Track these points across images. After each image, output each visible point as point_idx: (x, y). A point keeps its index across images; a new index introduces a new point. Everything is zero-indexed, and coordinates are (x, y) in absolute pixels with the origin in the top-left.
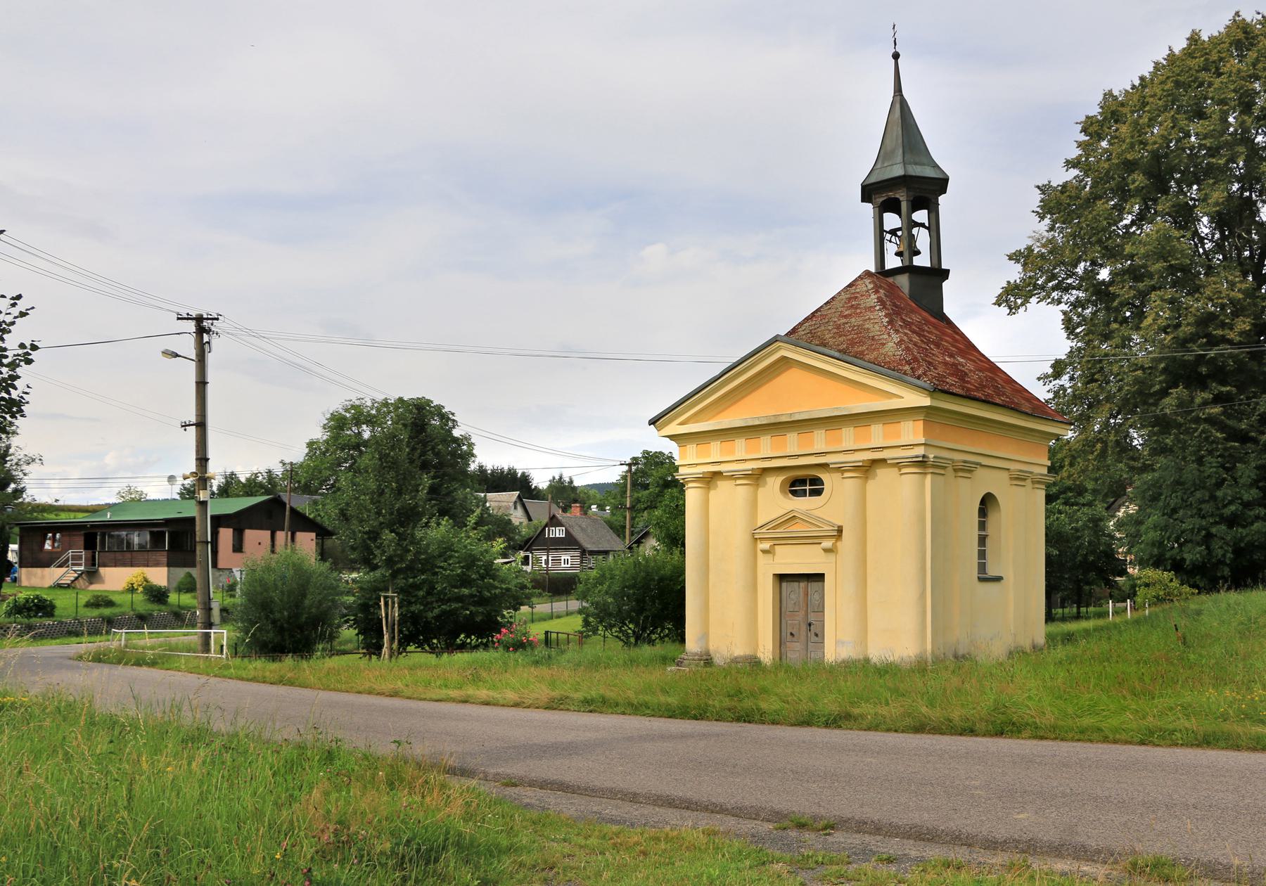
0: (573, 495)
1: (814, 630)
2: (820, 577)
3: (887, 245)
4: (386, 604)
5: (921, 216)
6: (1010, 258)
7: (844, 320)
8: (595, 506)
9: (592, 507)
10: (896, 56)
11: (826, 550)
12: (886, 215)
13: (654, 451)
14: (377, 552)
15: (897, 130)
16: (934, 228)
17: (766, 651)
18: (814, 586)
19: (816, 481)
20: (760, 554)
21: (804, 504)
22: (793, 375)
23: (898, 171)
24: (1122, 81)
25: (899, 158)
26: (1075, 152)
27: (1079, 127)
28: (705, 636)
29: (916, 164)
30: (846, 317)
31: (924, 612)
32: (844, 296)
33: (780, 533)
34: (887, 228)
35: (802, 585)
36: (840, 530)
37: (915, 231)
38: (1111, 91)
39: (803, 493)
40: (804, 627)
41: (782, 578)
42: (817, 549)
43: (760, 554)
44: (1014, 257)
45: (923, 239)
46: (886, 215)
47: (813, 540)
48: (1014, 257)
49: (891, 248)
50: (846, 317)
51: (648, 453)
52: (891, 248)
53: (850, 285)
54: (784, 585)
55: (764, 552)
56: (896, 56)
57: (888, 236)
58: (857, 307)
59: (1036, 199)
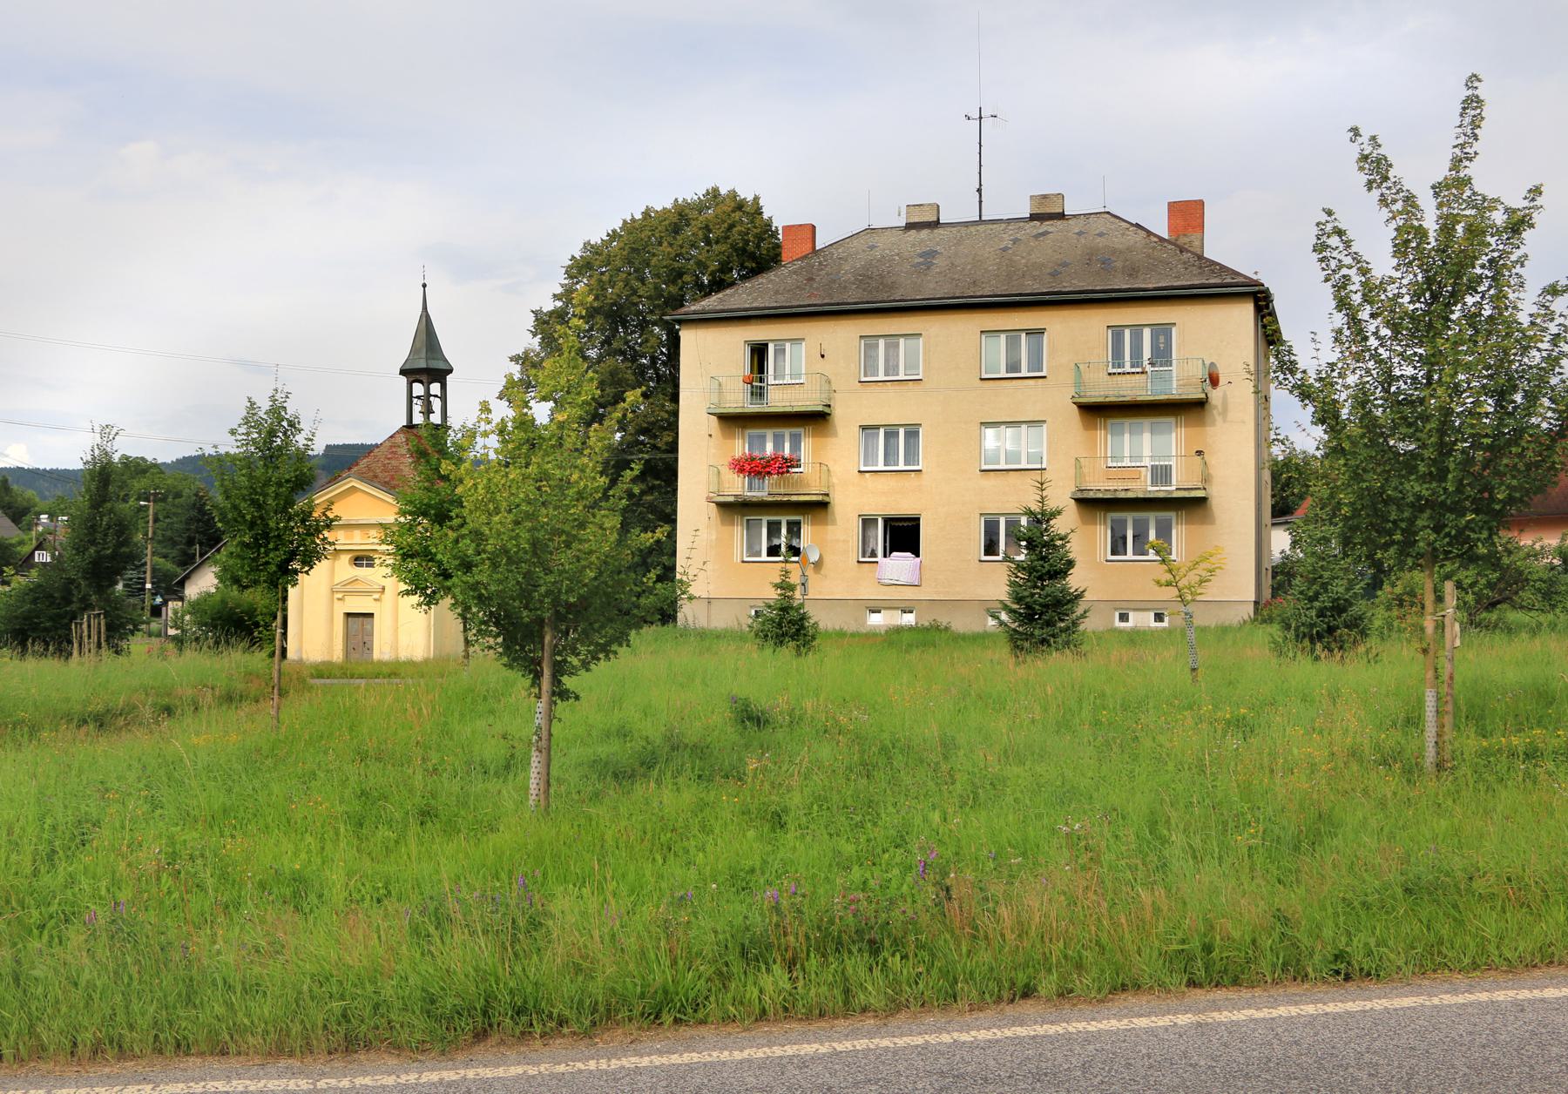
0: (7, 498)
1: (367, 645)
2: (371, 615)
3: (415, 407)
4: (76, 627)
5: (435, 388)
6: (511, 359)
7: (388, 461)
8: (46, 516)
9: (42, 516)
10: (424, 286)
11: (375, 600)
12: (415, 385)
13: (134, 456)
14: (75, 592)
15: (424, 336)
16: (443, 398)
17: (338, 655)
18: (367, 620)
19: (372, 559)
20: (336, 601)
21: (363, 572)
22: (359, 494)
23: (422, 364)
24: (597, 236)
25: (423, 355)
26: (559, 290)
27: (564, 270)
28: (300, 650)
29: (434, 359)
30: (389, 459)
31: (430, 636)
32: (388, 444)
33: (349, 588)
34: (414, 395)
35: (361, 619)
36: (384, 588)
37: (432, 399)
38: (589, 243)
39: (361, 565)
40: (361, 644)
41: (348, 615)
42: (370, 599)
43: (336, 601)
44: (515, 359)
45: (436, 404)
46: (415, 385)
47: (368, 593)
48: (515, 359)
49: (417, 408)
50: (389, 459)
51: (127, 458)
52: (417, 408)
53: (391, 437)
54: (350, 619)
55: (339, 599)
56: (424, 286)
57: (415, 400)
58: (395, 453)
59: (530, 321)
